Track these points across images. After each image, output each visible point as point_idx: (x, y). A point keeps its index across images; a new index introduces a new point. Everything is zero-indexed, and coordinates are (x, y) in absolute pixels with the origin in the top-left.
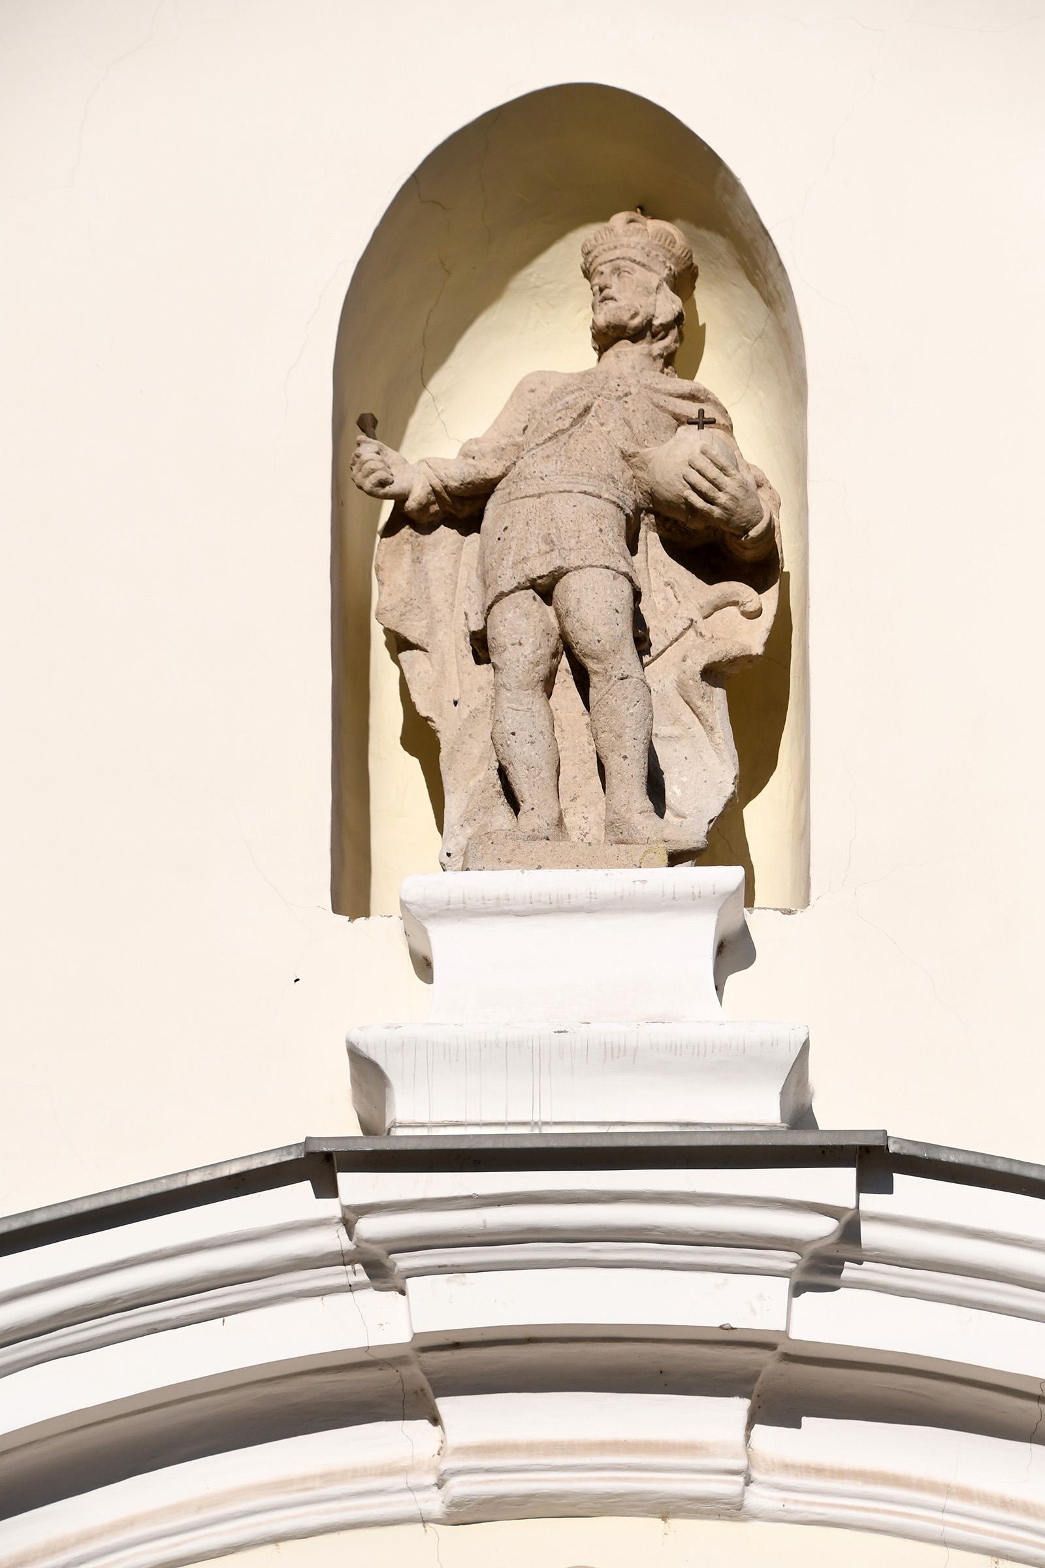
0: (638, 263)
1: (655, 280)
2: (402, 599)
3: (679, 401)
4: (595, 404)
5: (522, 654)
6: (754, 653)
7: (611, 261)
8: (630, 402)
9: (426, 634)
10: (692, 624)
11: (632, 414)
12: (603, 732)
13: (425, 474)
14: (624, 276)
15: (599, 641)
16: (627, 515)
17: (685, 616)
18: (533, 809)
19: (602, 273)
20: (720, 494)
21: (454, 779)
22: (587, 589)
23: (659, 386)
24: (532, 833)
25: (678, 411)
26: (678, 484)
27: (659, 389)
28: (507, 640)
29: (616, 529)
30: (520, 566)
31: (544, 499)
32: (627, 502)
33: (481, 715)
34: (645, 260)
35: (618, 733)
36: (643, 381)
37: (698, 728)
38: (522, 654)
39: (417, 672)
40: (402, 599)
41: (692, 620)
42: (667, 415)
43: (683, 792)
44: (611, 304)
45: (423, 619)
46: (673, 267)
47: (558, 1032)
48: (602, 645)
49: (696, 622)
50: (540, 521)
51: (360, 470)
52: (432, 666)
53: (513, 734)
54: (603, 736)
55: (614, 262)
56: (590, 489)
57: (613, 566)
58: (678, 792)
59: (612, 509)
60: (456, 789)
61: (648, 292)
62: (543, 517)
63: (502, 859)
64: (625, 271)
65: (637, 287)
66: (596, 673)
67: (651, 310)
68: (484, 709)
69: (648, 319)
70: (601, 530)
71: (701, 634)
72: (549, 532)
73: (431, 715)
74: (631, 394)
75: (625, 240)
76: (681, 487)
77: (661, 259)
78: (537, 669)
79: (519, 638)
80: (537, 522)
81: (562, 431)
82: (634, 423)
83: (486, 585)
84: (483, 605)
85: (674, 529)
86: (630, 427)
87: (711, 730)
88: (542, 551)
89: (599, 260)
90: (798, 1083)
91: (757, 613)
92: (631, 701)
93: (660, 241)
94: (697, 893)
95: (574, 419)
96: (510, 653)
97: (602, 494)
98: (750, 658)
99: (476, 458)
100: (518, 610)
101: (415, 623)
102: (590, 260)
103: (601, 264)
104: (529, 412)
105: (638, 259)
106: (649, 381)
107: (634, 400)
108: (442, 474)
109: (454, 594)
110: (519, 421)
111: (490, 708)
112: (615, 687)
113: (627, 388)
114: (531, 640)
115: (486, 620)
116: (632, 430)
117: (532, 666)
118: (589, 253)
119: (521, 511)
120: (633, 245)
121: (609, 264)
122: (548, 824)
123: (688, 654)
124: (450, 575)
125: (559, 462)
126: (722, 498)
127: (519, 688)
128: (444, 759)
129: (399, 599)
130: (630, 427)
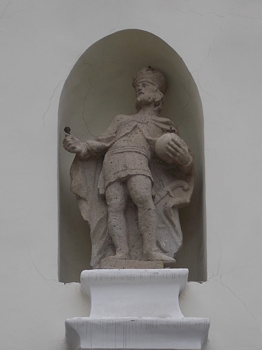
0: (150, 83)
1: (155, 88)
2: (78, 184)
3: (163, 125)
4: (138, 125)
5: (117, 202)
6: (187, 202)
7: (142, 82)
8: (149, 124)
9: (86, 195)
10: (168, 193)
11: (149, 128)
12: (143, 226)
13: (86, 145)
14: (146, 87)
15: (142, 198)
16: (148, 159)
17: (166, 190)
18: (121, 250)
19: (139, 86)
20: (177, 153)
21: (95, 240)
22: (137, 181)
23: (157, 120)
24: (121, 257)
25: (163, 127)
26: (165, 149)
27: (157, 121)
28: (112, 197)
29: (146, 163)
30: (116, 174)
31: (123, 154)
32: (149, 155)
33: (103, 220)
34: (152, 82)
35: (148, 226)
36: (152, 118)
37: (170, 225)
38: (117, 202)
39: (83, 207)
40: (78, 184)
41: (168, 191)
42: (160, 129)
43: (166, 245)
44: (142, 95)
45: (85, 190)
46: (160, 84)
47: (132, 321)
48: (143, 199)
49: (169, 192)
50: (122, 160)
51: (66, 144)
52: (88, 204)
53: (114, 226)
54: (143, 227)
55: (143, 83)
56: (138, 151)
57: (145, 174)
58: (164, 245)
59: (144, 157)
60: (95, 243)
61: (153, 91)
62: (123, 159)
63: (112, 265)
64: (146, 85)
65: (150, 90)
66: (141, 208)
67: (154, 97)
68: (104, 218)
69: (153, 99)
70: (141, 163)
71: (171, 196)
72: (125, 164)
73: (88, 220)
74: (149, 122)
75: (146, 76)
76: (165, 150)
77: (157, 82)
78: (122, 206)
79: (116, 196)
80: (122, 161)
81: (128, 133)
82: (150, 131)
83: (105, 180)
84: (104, 186)
85: (162, 163)
86: (149, 132)
87: (174, 226)
88: (123, 170)
89: (138, 82)
90: (206, 336)
91: (188, 190)
92: (152, 217)
93: (156, 76)
94: (174, 276)
95: (132, 129)
96: (113, 201)
97: (141, 153)
98: (186, 204)
99: (101, 141)
100: (116, 188)
101: (82, 191)
102: (135, 81)
103: (139, 83)
104: (117, 127)
105: (150, 82)
106: (154, 118)
107: (150, 124)
108: (91, 145)
109: (94, 183)
110: (114, 130)
111: (106, 218)
112: (147, 212)
113: (148, 120)
114: (120, 197)
115: (105, 191)
116: (150, 133)
117: (120, 205)
118: (135, 80)
119: (116, 157)
120: (148, 77)
121: (141, 83)
122: (125, 255)
123: (167, 202)
124: (93, 176)
125: (128, 143)
126: (178, 154)
127: (116, 212)
128: (92, 234)
129: (78, 184)
130: (149, 132)
